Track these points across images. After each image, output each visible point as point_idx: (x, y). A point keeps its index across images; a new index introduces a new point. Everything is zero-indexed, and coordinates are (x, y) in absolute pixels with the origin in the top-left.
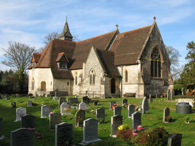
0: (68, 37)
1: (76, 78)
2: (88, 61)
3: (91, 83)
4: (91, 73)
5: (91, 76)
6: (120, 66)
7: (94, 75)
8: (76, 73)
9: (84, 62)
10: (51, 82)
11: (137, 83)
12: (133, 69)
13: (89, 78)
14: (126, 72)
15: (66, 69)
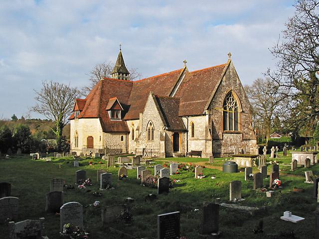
1: (133, 131)
15: (119, 119)
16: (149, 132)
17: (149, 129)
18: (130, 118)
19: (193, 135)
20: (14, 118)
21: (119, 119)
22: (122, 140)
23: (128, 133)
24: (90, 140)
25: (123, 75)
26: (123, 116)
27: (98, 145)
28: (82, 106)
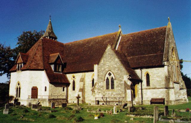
0: (53, 38)
1: (74, 82)
2: (102, 61)
3: (107, 88)
4: (107, 76)
5: (108, 79)
6: (137, 68)
7: (112, 78)
8: (74, 77)
9: (95, 64)
10: (46, 87)
11: (164, 87)
12: (157, 72)
13: (105, 82)
14: (148, 76)
15: (60, 72)
16: (17, 90)
17: (108, 79)
18: (68, 71)
19: (148, 83)
20: (9, 48)
21: (60, 72)
22: (64, 90)
23: (68, 84)
24: (35, 91)
25: (52, 39)
26: (63, 70)
27: (43, 95)
28: (25, 59)
